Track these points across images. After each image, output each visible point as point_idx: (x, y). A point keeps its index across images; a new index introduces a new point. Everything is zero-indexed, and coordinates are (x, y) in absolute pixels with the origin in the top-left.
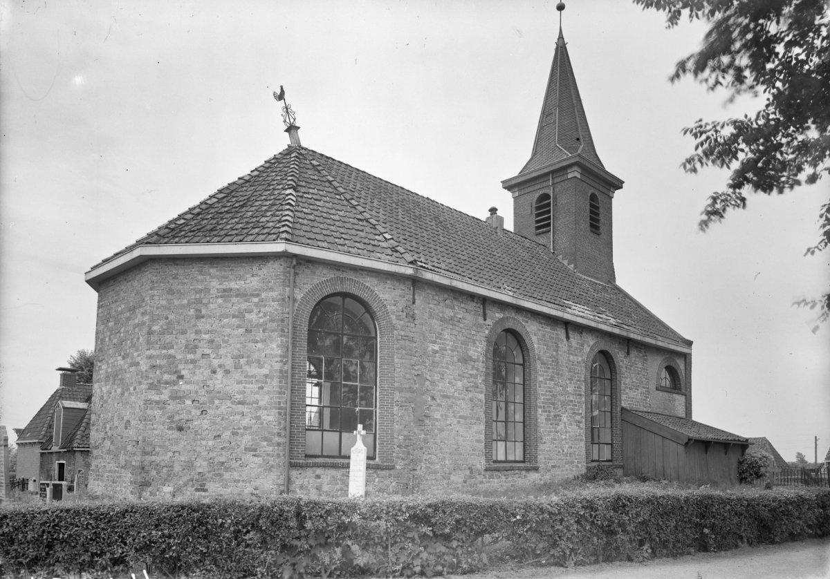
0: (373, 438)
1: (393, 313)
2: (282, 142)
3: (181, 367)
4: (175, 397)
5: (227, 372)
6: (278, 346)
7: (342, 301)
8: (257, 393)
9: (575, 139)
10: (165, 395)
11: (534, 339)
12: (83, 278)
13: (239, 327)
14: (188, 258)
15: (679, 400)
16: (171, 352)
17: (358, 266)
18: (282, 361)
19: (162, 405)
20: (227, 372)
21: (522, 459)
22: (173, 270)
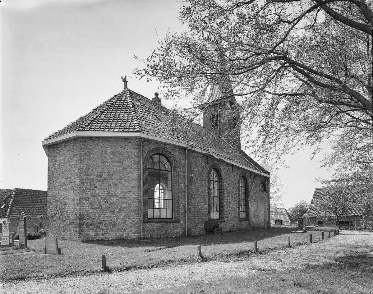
0: (150, 209)
1: (178, 161)
2: (120, 88)
3: (95, 183)
4: (93, 195)
5: (116, 185)
6: (137, 175)
7: (159, 157)
8: (128, 194)
9: (121, 87)
10: (89, 194)
11: (223, 172)
12: (41, 145)
13: (120, 167)
14: (82, 137)
15: (266, 194)
16: (90, 176)
17: (166, 143)
18: (139, 181)
19: (87, 199)
20: (116, 185)
21: (219, 218)
22: (90, 143)
